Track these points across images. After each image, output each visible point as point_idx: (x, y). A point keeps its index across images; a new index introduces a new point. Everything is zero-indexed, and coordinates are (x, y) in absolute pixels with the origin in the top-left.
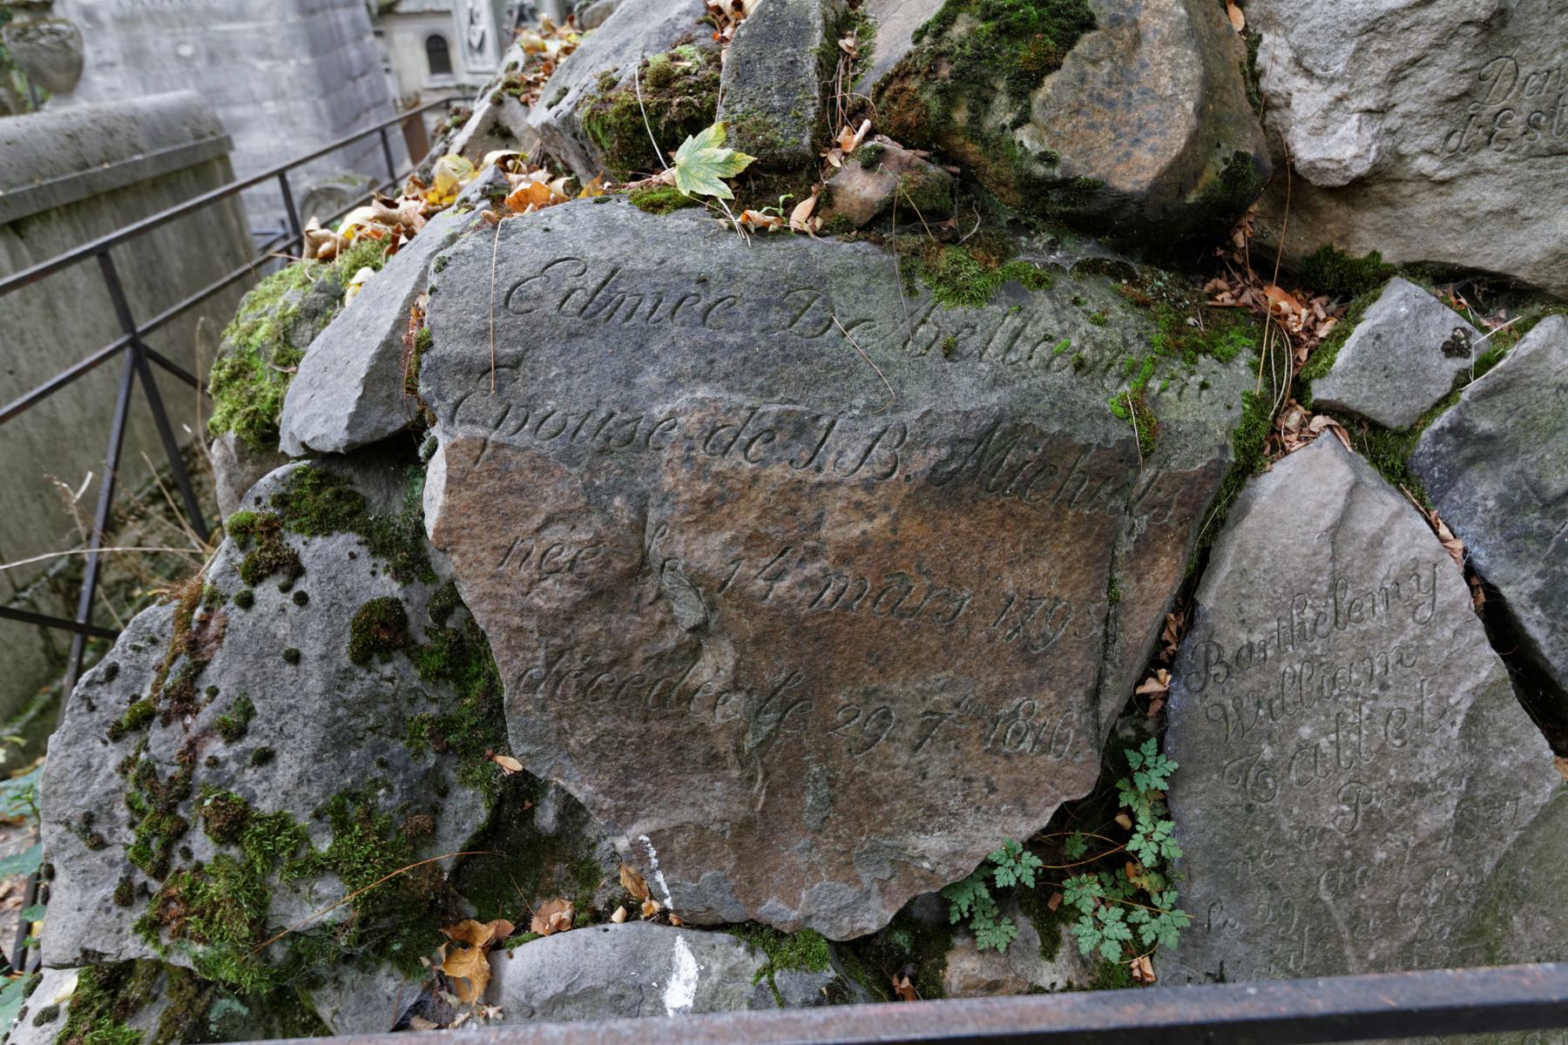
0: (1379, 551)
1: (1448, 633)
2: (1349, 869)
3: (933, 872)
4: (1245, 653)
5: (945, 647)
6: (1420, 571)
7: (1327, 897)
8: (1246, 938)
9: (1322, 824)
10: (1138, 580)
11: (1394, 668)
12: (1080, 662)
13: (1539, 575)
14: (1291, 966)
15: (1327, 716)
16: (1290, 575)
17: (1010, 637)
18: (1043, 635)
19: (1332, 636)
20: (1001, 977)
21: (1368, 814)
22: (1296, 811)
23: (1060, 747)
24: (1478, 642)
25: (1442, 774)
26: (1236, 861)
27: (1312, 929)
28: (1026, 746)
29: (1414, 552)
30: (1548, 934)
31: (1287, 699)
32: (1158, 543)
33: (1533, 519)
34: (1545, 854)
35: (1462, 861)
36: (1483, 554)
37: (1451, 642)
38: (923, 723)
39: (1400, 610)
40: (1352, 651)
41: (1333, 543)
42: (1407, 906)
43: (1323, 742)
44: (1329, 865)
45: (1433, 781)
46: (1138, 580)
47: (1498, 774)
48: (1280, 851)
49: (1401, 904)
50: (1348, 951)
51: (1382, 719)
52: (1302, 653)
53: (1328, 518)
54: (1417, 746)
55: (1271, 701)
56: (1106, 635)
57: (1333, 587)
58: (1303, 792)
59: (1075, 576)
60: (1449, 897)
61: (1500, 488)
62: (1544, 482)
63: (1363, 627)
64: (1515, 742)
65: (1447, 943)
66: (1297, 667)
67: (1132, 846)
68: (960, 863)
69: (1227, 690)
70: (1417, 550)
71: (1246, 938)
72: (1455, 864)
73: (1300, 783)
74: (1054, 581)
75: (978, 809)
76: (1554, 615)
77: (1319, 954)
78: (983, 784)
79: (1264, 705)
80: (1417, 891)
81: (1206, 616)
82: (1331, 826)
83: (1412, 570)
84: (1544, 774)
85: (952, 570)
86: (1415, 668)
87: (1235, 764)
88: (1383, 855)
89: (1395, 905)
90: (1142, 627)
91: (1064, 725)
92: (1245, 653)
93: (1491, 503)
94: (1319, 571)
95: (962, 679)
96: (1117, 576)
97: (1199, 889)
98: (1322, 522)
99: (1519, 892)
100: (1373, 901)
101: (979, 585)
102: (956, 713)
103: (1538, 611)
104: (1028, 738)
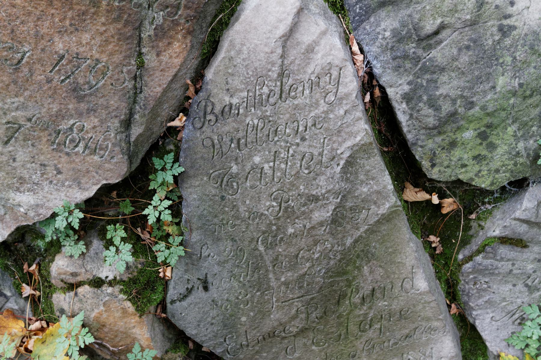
0: (311, 55)
1: (342, 112)
2: (273, 236)
3: (26, 214)
4: (227, 109)
5: (15, 82)
6: (332, 71)
7: (261, 248)
8: (219, 263)
9: (261, 211)
10: (158, 55)
11: (310, 129)
12: (117, 103)
13: (409, 83)
14: (242, 279)
15: (270, 152)
16: (257, 64)
17: (63, 81)
18: (88, 83)
19: (277, 105)
20: (78, 271)
21: (286, 208)
22: (248, 202)
23: (102, 152)
24: (359, 119)
25: (328, 192)
26: (215, 224)
27: (252, 263)
28: (80, 149)
29: (329, 59)
30: (381, 276)
31: (248, 139)
32: (172, 33)
33: (411, 48)
34: (386, 238)
35: (334, 238)
36: (378, 66)
37: (343, 117)
38: (7, 129)
39: (318, 94)
40: (288, 116)
41: (284, 47)
42: (303, 257)
43: (266, 166)
44: (264, 233)
45: (323, 195)
46: (158, 55)
47: (361, 195)
48: (238, 222)
49: (300, 256)
50: (271, 276)
51: (300, 157)
52: (259, 113)
53: (283, 29)
54: (317, 175)
55: (239, 140)
56: (135, 88)
57: (281, 75)
58: (252, 192)
59: (110, 47)
60: (325, 255)
61: (396, 24)
62: (422, 24)
63: (296, 102)
64: (373, 179)
65: (321, 277)
66: (256, 122)
67: (146, 212)
68: (41, 211)
69: (215, 130)
70: (331, 57)
71: (219, 263)
72: (330, 239)
73: (251, 187)
74: (95, 48)
75: (51, 182)
76: (412, 109)
77: (256, 276)
78: (53, 168)
79: (235, 141)
80: (309, 250)
81: (207, 83)
82: (266, 212)
83: (327, 71)
84: (386, 198)
85: (13, 31)
86: (322, 130)
87: (216, 173)
88: (293, 231)
89: (297, 256)
90: (160, 86)
91: (105, 140)
92: (227, 109)
93: (388, 34)
94: (273, 64)
95: (30, 104)
96: (144, 50)
97: (195, 237)
98: (278, 32)
99: (370, 255)
100: (286, 253)
101: (36, 44)
102: (29, 125)
103: (404, 105)
104: (81, 145)
